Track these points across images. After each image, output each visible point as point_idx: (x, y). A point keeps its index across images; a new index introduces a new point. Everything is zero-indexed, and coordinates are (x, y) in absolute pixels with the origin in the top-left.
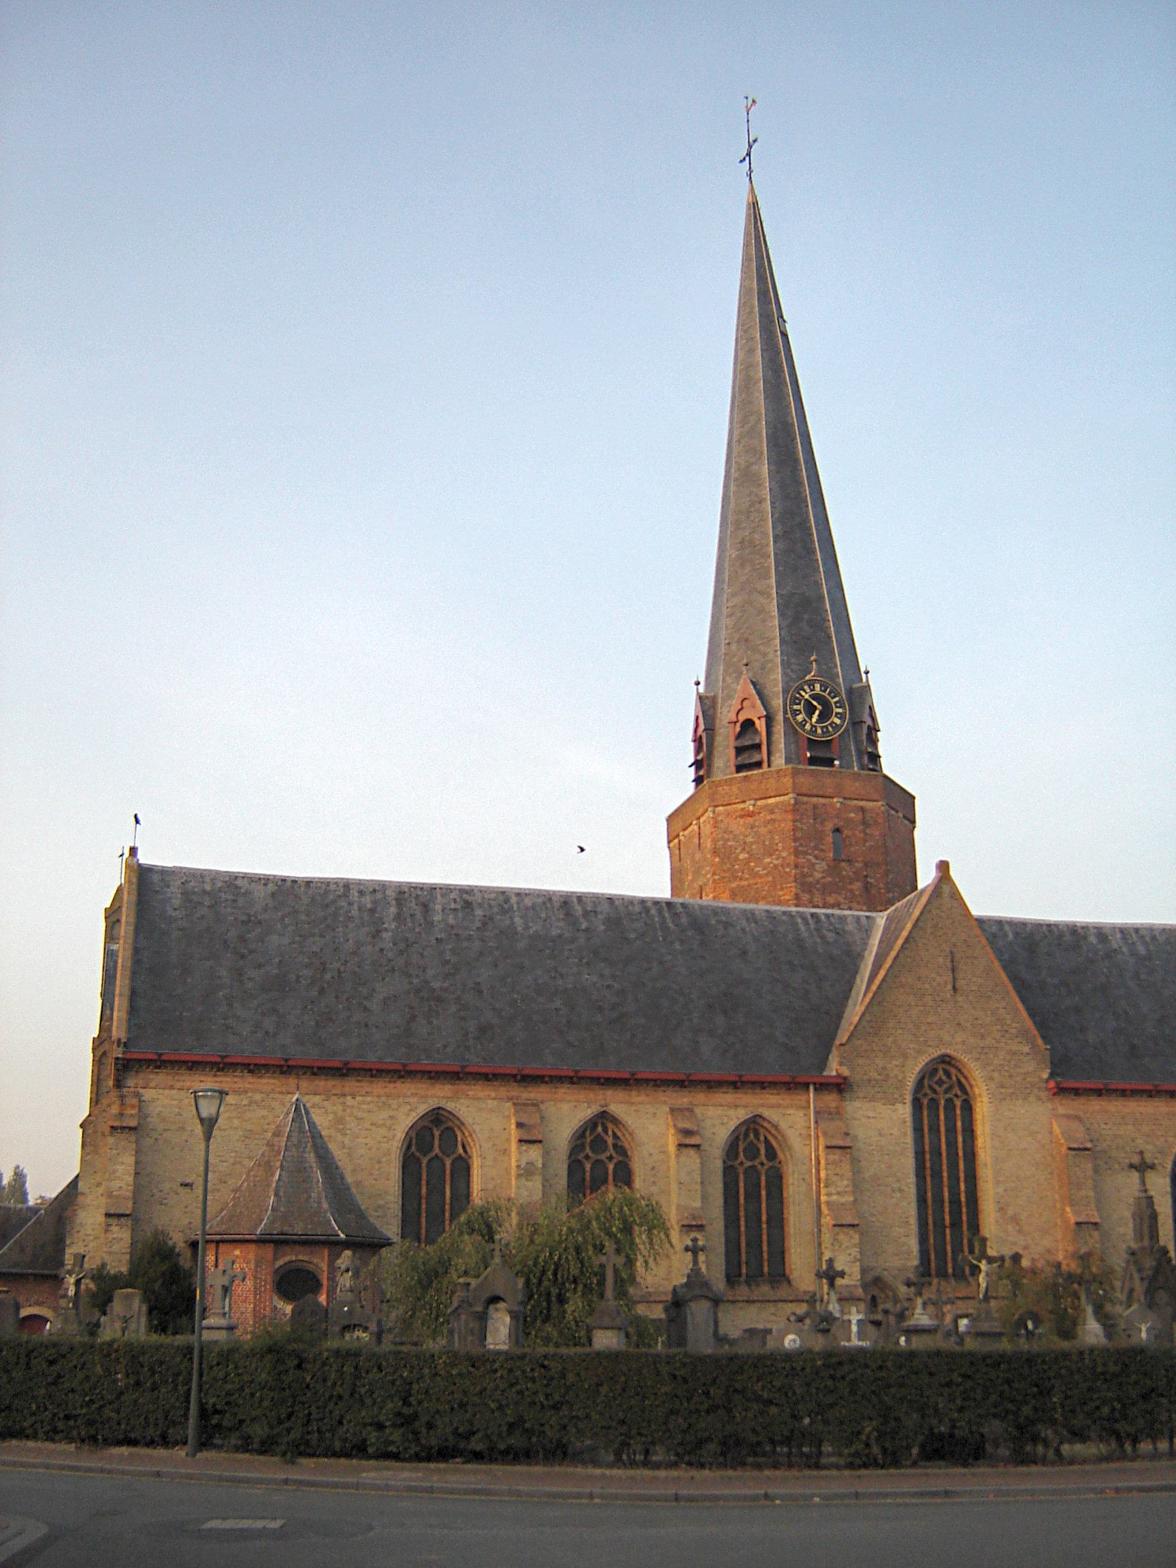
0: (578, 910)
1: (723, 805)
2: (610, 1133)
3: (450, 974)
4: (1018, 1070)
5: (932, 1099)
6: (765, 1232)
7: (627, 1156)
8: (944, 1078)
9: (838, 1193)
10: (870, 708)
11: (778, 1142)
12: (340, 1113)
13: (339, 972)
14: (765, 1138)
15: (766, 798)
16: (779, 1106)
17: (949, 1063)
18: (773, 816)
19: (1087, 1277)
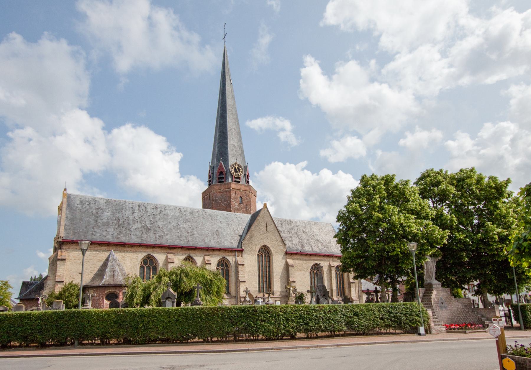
0: (183, 210)
11: (228, 263)
12: (124, 256)
13: (123, 222)
16: (229, 255)
17: (265, 247)
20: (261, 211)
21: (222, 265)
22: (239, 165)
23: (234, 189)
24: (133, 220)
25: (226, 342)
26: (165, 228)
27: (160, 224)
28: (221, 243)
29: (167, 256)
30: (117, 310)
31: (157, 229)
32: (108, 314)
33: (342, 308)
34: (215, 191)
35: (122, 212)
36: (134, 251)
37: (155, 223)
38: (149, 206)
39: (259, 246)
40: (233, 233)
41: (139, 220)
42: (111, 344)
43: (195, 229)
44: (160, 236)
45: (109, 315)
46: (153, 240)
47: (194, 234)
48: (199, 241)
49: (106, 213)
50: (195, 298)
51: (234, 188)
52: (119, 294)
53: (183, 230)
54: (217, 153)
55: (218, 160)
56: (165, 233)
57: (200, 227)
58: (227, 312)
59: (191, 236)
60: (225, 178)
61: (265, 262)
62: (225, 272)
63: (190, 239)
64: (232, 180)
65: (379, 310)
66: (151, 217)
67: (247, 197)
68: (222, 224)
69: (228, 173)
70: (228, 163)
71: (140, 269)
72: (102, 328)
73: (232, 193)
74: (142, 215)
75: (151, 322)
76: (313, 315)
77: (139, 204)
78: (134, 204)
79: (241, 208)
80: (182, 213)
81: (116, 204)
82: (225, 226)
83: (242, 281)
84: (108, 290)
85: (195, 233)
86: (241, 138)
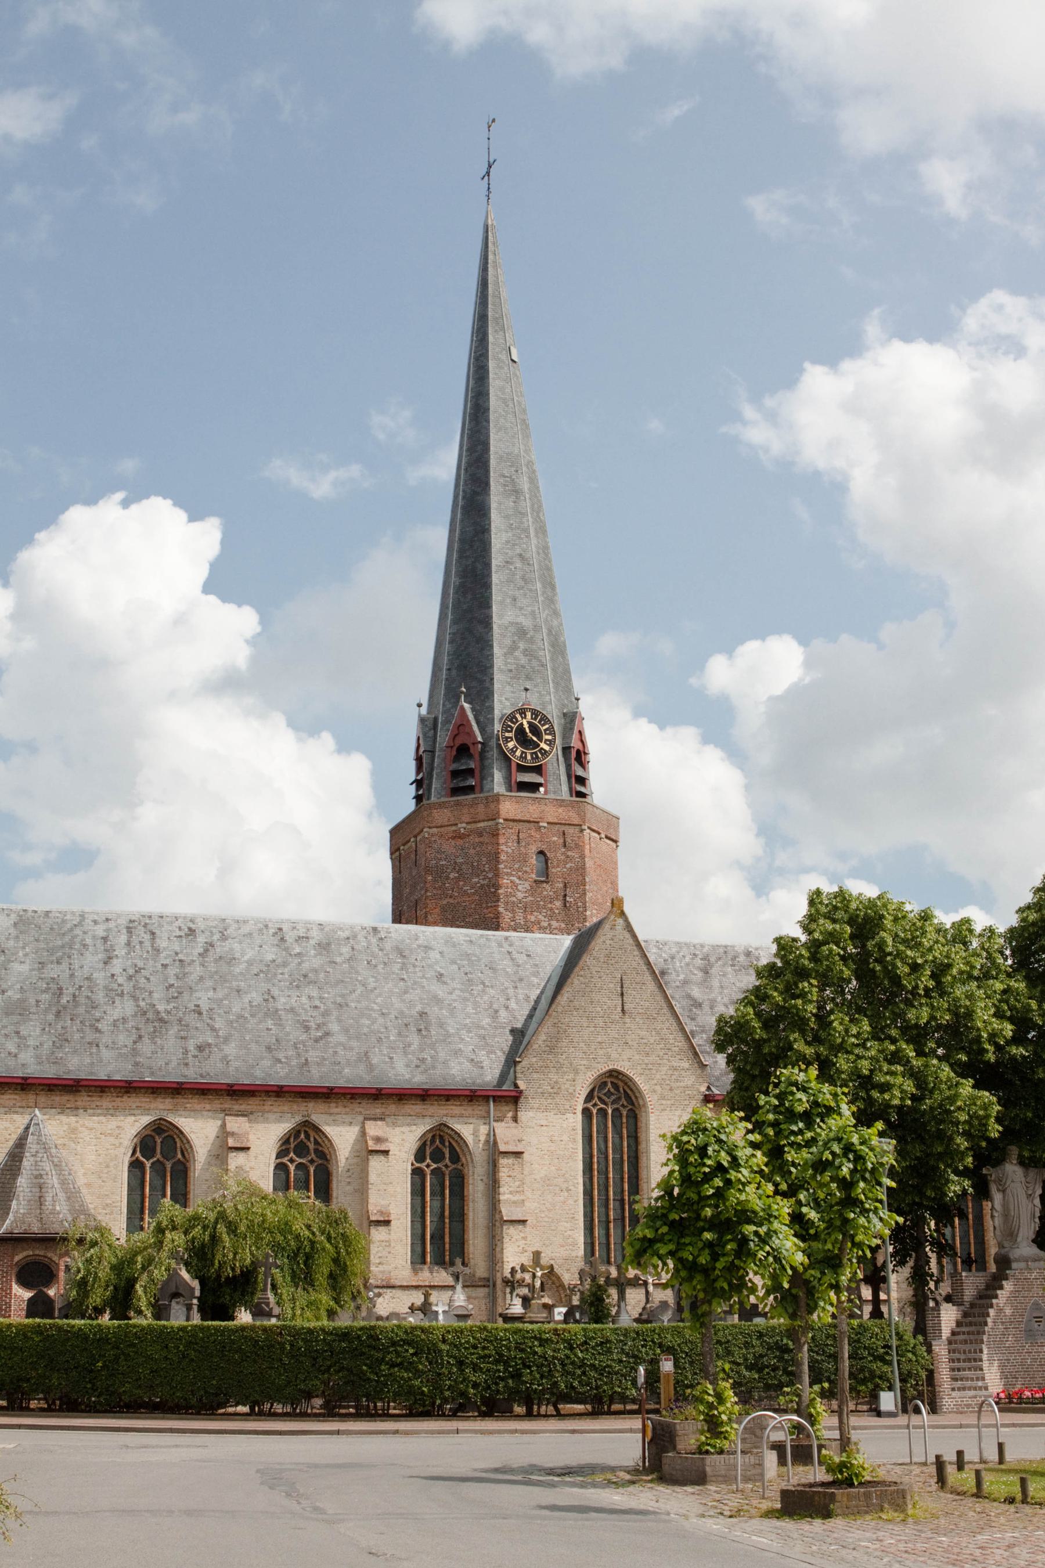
0: (290, 937)
1: (437, 827)
2: (312, 1139)
3: (173, 998)
4: (678, 1084)
5: (600, 1110)
6: (447, 1226)
7: (327, 1160)
8: (612, 1090)
9: (511, 1193)
10: (580, 732)
11: (460, 1147)
12: (73, 1125)
13: (74, 996)
14: (450, 1143)
15: (475, 822)
16: (461, 1116)
17: (617, 1077)
18: (481, 839)
19: (622, 1280)
20: (600, 932)
21: (437, 1156)
22: (535, 713)
23: (514, 821)
24: (106, 988)
25: (304, 1416)
26: (219, 1015)
27: (203, 998)
28: (434, 1067)
29: (224, 1126)
30: (45, 1324)
31: (191, 1019)
32: (23, 1332)
33: (625, 1335)
34: (435, 830)
35: (69, 957)
36: (108, 1109)
37: (186, 996)
38: (166, 927)
39: (589, 1074)
40: (486, 1021)
41: (128, 987)
42: (33, 1410)
43: (335, 1013)
44: (200, 1048)
45: (25, 1335)
46: (174, 1064)
47: (327, 1034)
48: (348, 1063)
49: (16, 967)
50: (259, 1295)
51: (511, 816)
52: (57, 1265)
53: (288, 1019)
54: (451, 662)
55: (452, 696)
56: (221, 1033)
57: (353, 1005)
58: (304, 1340)
59: (316, 1041)
60: (477, 772)
61: (617, 1140)
62: (447, 1183)
63: (313, 1055)
64: (508, 779)
65: (747, 1342)
66: (172, 971)
67: (570, 849)
68: (445, 983)
69: (492, 750)
70: (491, 709)
71: (129, 1171)
72: (11, 1368)
73: (502, 840)
74: (140, 964)
75: (122, 1357)
76: (536, 1353)
77: (131, 921)
78: (112, 924)
79: (544, 899)
80: (286, 949)
81: (52, 929)
82: (457, 992)
83: (514, 1218)
84: (24, 1250)
85: (334, 1027)
86: (553, 587)
